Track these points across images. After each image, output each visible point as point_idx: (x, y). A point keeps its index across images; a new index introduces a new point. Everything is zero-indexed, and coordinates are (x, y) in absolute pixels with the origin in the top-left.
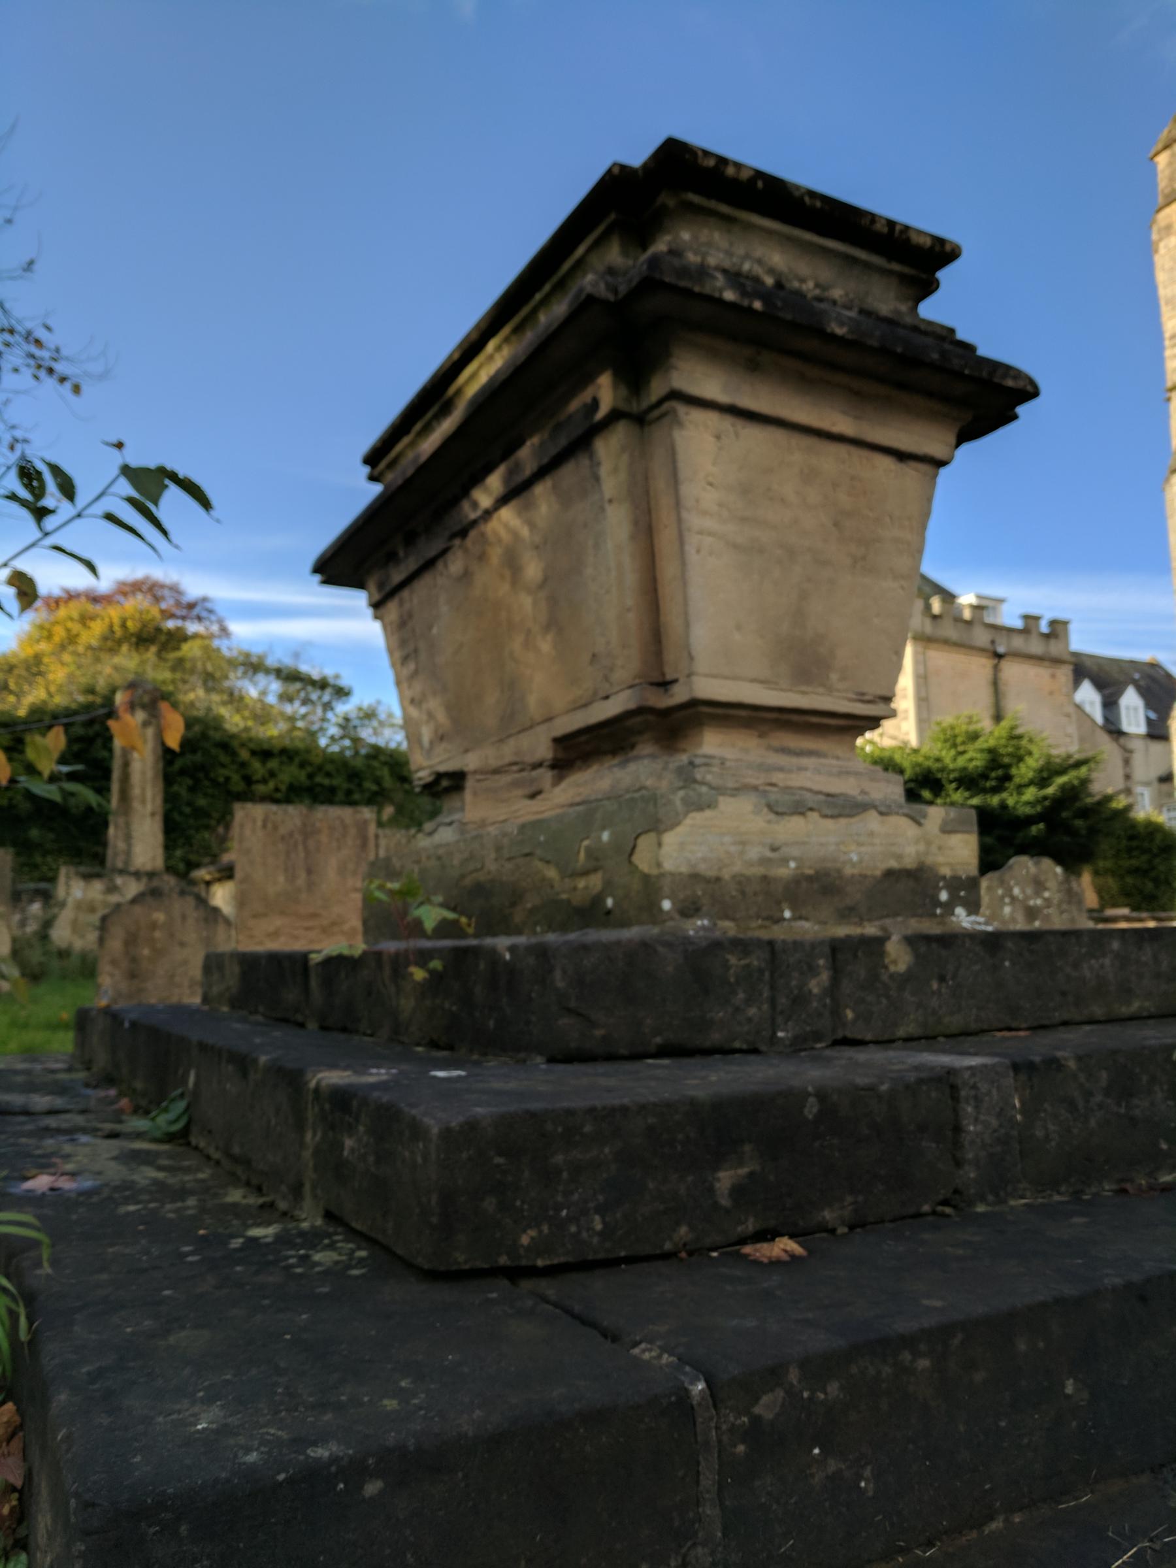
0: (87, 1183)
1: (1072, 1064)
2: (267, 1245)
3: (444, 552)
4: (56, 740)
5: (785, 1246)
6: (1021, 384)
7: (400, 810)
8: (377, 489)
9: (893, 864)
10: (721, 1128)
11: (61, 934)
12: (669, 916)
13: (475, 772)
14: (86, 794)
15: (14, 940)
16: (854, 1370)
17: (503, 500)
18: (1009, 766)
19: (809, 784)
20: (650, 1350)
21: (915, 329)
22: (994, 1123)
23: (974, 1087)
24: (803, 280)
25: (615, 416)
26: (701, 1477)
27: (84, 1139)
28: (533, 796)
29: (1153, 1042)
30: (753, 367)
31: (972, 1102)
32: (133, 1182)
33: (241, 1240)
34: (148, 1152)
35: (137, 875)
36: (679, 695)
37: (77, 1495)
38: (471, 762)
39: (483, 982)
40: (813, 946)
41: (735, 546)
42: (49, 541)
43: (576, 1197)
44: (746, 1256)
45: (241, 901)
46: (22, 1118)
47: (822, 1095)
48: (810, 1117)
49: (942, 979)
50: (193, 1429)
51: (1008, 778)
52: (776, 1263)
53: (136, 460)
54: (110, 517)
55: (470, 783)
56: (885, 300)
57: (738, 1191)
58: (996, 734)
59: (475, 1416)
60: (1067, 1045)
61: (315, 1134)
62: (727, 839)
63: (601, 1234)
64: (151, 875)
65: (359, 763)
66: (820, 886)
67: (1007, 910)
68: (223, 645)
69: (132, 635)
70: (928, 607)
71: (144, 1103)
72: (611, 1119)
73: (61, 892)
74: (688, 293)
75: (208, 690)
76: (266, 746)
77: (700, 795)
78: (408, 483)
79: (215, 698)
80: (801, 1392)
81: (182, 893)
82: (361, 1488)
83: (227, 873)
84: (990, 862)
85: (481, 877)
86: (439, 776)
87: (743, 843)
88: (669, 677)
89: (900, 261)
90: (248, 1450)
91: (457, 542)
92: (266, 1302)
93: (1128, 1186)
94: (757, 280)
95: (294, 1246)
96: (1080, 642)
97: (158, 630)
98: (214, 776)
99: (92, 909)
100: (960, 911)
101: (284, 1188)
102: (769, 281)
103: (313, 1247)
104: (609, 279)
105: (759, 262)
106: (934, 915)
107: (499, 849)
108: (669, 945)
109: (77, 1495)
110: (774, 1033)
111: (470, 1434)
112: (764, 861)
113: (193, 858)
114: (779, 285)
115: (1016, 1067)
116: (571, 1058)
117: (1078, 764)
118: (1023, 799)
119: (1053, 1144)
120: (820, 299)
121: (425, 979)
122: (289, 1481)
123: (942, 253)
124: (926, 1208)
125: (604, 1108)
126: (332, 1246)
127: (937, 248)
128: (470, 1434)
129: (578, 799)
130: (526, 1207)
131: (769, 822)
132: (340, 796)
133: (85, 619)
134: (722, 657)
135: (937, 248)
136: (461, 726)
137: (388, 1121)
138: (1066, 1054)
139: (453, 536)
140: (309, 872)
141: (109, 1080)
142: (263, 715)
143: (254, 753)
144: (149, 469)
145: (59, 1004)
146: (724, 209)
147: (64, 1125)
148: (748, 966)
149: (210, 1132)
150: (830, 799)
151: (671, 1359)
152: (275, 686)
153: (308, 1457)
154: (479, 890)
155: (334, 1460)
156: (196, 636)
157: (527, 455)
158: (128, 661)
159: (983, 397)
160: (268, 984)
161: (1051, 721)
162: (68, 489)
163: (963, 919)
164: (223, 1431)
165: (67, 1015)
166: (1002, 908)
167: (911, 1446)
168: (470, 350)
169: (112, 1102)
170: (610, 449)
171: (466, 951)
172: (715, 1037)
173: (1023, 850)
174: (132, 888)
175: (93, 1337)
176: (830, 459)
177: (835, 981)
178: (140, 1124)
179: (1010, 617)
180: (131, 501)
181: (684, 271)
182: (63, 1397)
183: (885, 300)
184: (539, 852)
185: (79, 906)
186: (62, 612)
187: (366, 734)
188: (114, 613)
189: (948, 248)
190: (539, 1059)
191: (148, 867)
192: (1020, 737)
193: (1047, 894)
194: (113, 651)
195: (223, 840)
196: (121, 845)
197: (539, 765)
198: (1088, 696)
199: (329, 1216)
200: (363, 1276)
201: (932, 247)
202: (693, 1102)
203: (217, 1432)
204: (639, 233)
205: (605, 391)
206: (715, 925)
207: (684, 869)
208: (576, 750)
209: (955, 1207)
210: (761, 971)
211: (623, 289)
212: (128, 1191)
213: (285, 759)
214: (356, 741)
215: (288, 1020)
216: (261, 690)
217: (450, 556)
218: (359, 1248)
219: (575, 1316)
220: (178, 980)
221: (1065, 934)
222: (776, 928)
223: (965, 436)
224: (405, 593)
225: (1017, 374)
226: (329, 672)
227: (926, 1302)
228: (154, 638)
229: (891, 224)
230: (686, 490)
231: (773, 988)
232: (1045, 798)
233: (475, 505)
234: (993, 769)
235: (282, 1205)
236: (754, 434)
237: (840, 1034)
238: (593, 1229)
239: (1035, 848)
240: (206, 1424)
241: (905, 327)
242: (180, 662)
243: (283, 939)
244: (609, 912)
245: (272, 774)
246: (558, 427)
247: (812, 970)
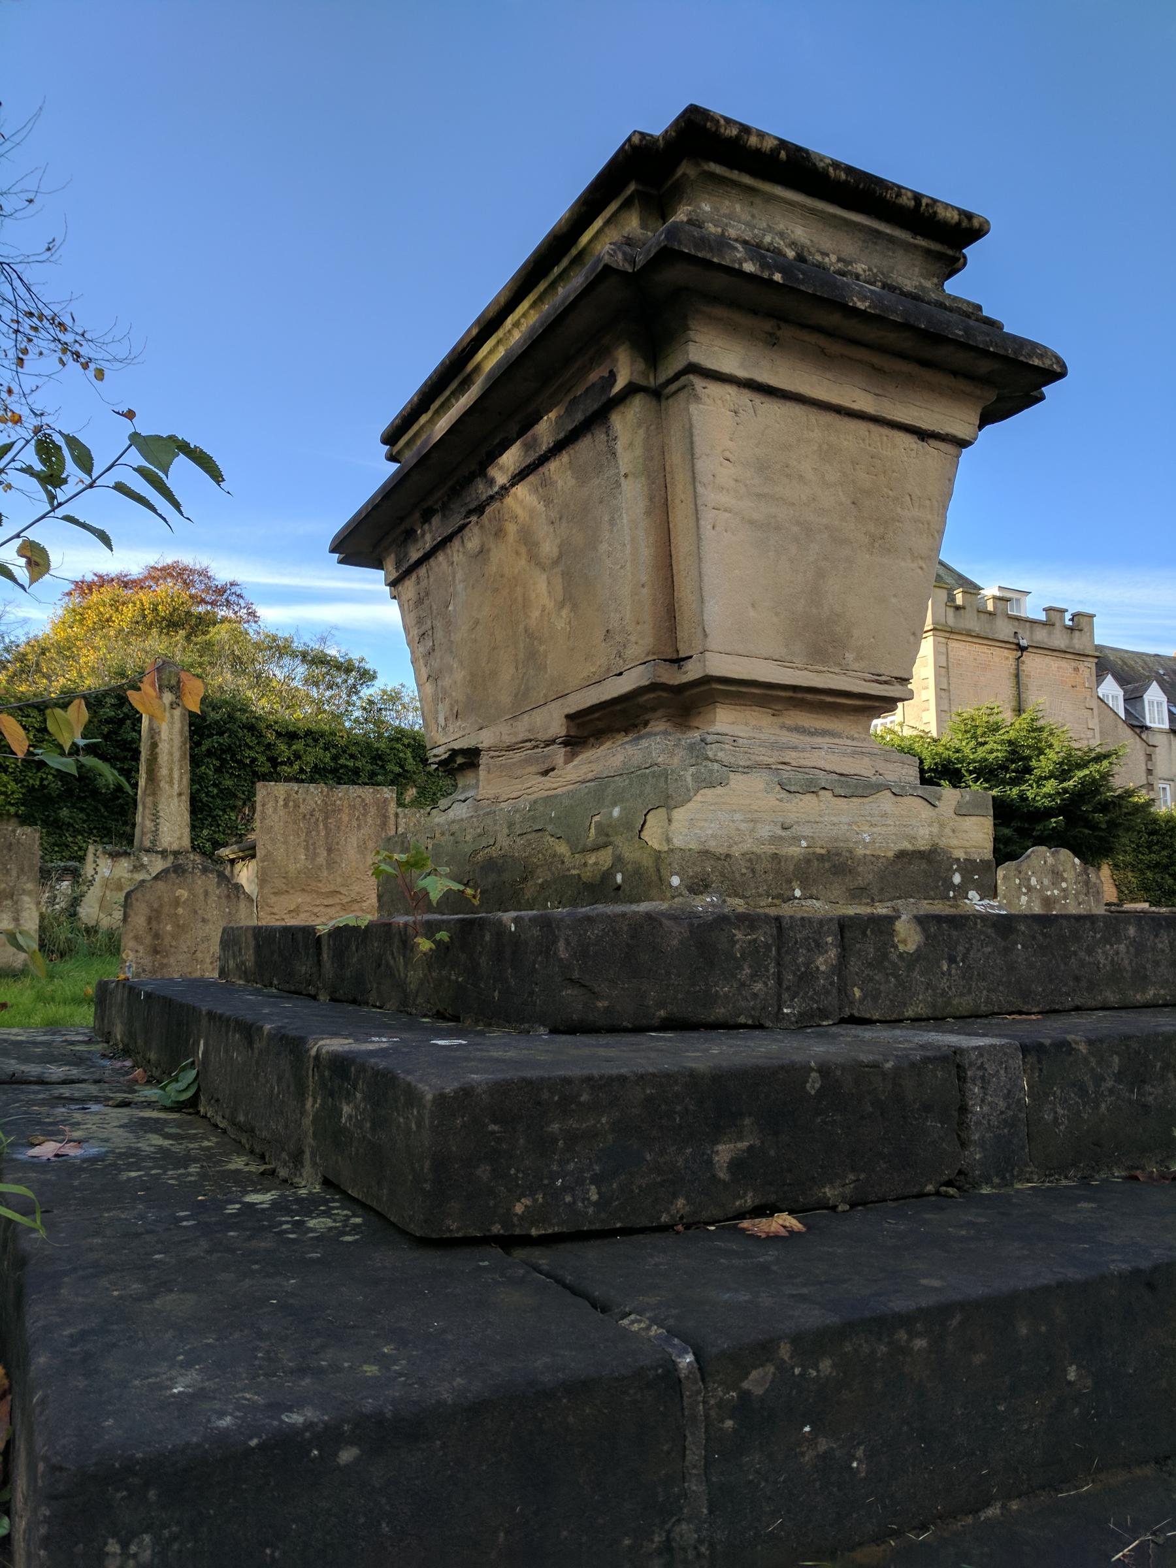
0: (93, 1150)
1: (1083, 1048)
2: (264, 1210)
3: (462, 528)
4: (78, 714)
5: (784, 1221)
6: (1047, 363)
7: (422, 792)
8: (394, 467)
9: (907, 846)
10: (721, 1100)
11: (89, 911)
12: (676, 893)
13: (489, 749)
14: (109, 775)
15: (42, 917)
16: (848, 1348)
17: (520, 476)
18: (1029, 758)
19: (822, 764)
20: (640, 1321)
21: (940, 305)
22: (1002, 1104)
23: (981, 1067)
24: (825, 254)
25: (632, 389)
26: (688, 1452)
27: (95, 1108)
28: (545, 773)
29: (1168, 1029)
30: (772, 342)
31: (979, 1082)
32: (138, 1149)
33: (238, 1206)
34: (157, 1120)
35: (164, 853)
36: (692, 671)
37: (46, 1459)
38: (485, 739)
39: (489, 952)
40: (821, 923)
41: (751, 522)
42: (60, 512)
43: (571, 1166)
44: (744, 1230)
45: (262, 879)
46: (37, 1087)
47: (824, 1070)
48: (813, 1092)
49: (952, 960)
50: (168, 1392)
51: (1028, 770)
52: (773, 1238)
53: (146, 429)
54: (120, 488)
55: (484, 760)
56: (910, 275)
57: (736, 1165)
58: (1017, 726)
59: (455, 1384)
60: (1077, 1030)
61: (315, 1102)
63: (596, 1204)
64: (176, 854)
65: (382, 745)
66: (832, 865)
67: (1024, 899)
68: (251, 629)
69: (164, 618)
70: (952, 598)
71: (157, 1073)
72: (607, 1088)
73: (88, 869)
74: (707, 264)
75: (234, 672)
76: (291, 728)
77: (711, 771)
78: (423, 461)
79: (243, 681)
80: (793, 1368)
81: (205, 870)
82: (336, 1455)
83: (250, 853)
84: (1005, 851)
85: (494, 852)
86: (454, 753)
88: (682, 655)
89: (925, 236)
90: (222, 1414)
91: (474, 519)
92: (256, 1267)
93: (1138, 1173)
94: (778, 252)
95: (290, 1212)
96: (1104, 635)
97: (188, 613)
98: (236, 755)
99: (120, 888)
100: (972, 894)
101: (284, 1155)
102: (791, 254)
103: (309, 1214)
104: (627, 249)
105: (781, 235)
106: (948, 898)
107: (511, 825)
108: (675, 918)
109: (46, 1459)
110: (780, 1009)
111: (450, 1401)
112: (774, 839)
113: (219, 837)
114: (801, 258)
115: (1025, 1049)
116: (572, 1029)
117: (1099, 759)
118: (1042, 792)
119: (1062, 1128)
120: (843, 274)
121: (431, 949)
122: (261, 1447)
123: (967, 231)
124: (930, 1188)
125: (601, 1077)
126: (327, 1214)
127: (965, 224)
128: (450, 1401)
129: (590, 776)
130: (520, 1175)
132: (364, 777)
133: (116, 604)
134: (736, 635)
135: (965, 224)
136: (472, 706)
137: (384, 1087)
138: (1078, 1038)
139: (470, 513)
140: (330, 851)
141: (127, 1052)
142: (291, 700)
143: (279, 734)
144: (160, 437)
145: (81, 979)
146: (747, 180)
147: (77, 1095)
148: (755, 940)
149: (217, 1100)
150: (843, 778)
151: (661, 1330)
152: (301, 670)
153: (282, 1421)
154: (491, 866)
155: (309, 1425)
156: (224, 620)
157: (545, 430)
158: (157, 643)
159: (1009, 378)
160: (283, 958)
161: (1073, 715)
162: (85, 460)
163: (975, 902)
164: (200, 1395)
165: (90, 990)
166: (1019, 898)
167: (905, 1428)
168: (489, 326)
169: (127, 1073)
170: (627, 424)
171: (471, 922)
172: (720, 1012)
173: (1040, 841)
174: (158, 865)
175: (80, 1299)
176: (852, 435)
177: (843, 958)
178: (151, 1093)
179: (1032, 609)
180: (140, 470)
181: (704, 242)
182: (42, 1360)
183: (910, 275)
184: (549, 828)
185: (106, 884)
186: (95, 597)
187: (389, 716)
188: (145, 597)
189: (976, 223)
190: (542, 1030)
191: (175, 847)
192: (1040, 730)
193: (1064, 885)
194: (145, 635)
195: (250, 820)
196: (149, 824)
197: (553, 742)
198: (1111, 689)
199: (327, 1183)
200: (356, 1241)
201: (959, 224)
202: (692, 1074)
203: (193, 1396)
204: (658, 204)
205: (625, 370)
206: (724, 901)
207: (694, 846)
208: (591, 726)
209: (959, 1188)
210: (768, 947)
211: (641, 260)
212: (133, 1157)
213: (310, 741)
214: (378, 723)
215: (299, 992)
216: (289, 674)
217: (466, 531)
218: (355, 1215)
219: (565, 1286)
220: (197, 956)
221: (1079, 918)
222: (785, 906)
223: (987, 419)
224: (422, 571)
225: (1044, 352)
226: (355, 656)
227: (924, 1282)
228: (186, 622)
229: (917, 197)
230: (701, 465)
231: (778, 964)
232: (1065, 791)
233: (492, 482)
234: (1013, 762)
235: (283, 1173)
236: (773, 411)
237: (847, 1012)
238: (588, 1199)
239: (1053, 840)
240: (186, 1387)
241: (929, 303)
242: (209, 645)
243: (303, 916)
244: (619, 888)
245: (298, 757)
246: (574, 402)
247: (820, 947)
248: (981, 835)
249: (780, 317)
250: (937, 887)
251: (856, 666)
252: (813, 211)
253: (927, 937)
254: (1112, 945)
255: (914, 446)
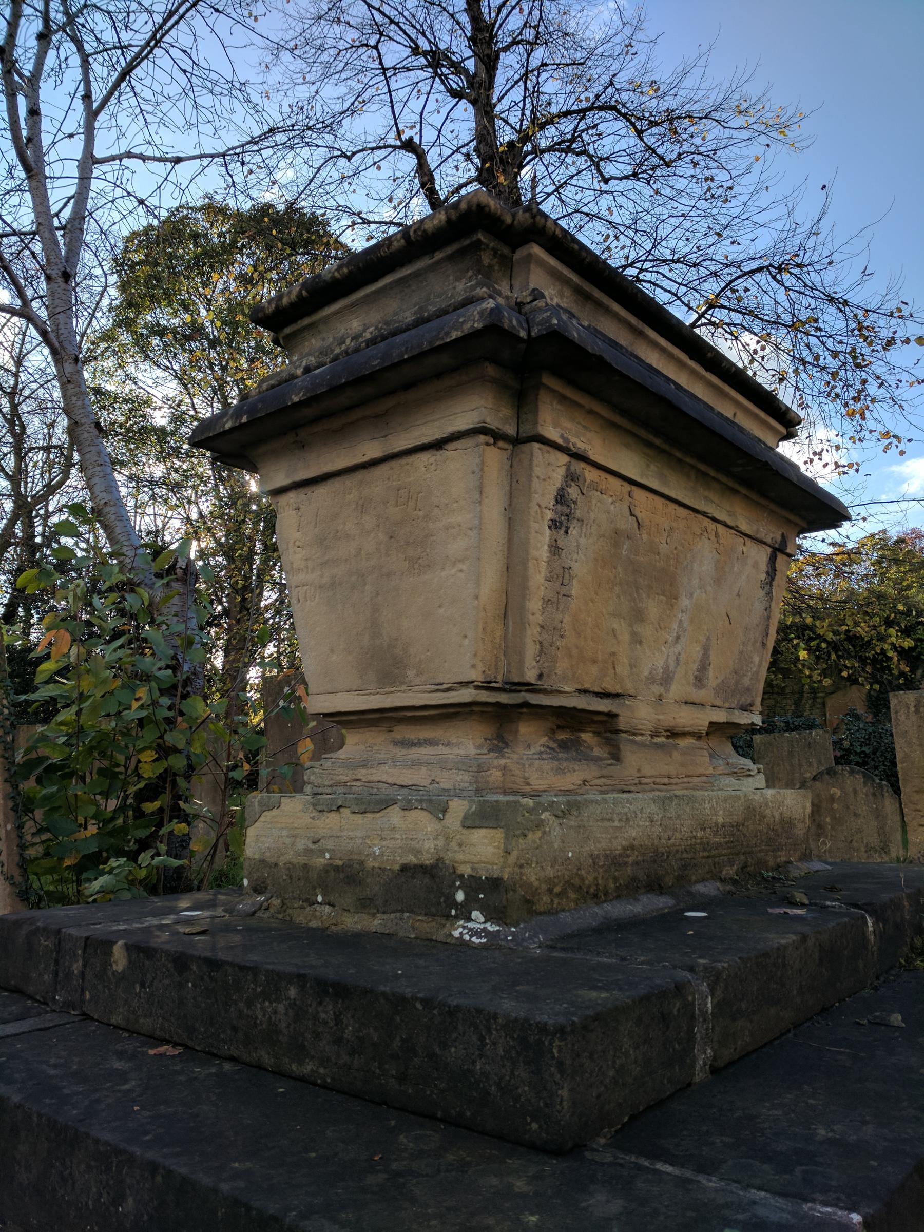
9: (412, 859)
19: (384, 778)
30: (302, 446)
49: (143, 985)
62: (285, 833)
87: (295, 836)
112: (308, 852)
131: (313, 818)
146: (306, 321)
176: (378, 482)
177: (85, 966)
236: (321, 491)
248: (491, 850)
249: (296, 427)
250: (439, 904)
251: (417, 681)
252: (353, 305)
253: (130, 962)
254: (271, 1003)
255: (432, 460)
